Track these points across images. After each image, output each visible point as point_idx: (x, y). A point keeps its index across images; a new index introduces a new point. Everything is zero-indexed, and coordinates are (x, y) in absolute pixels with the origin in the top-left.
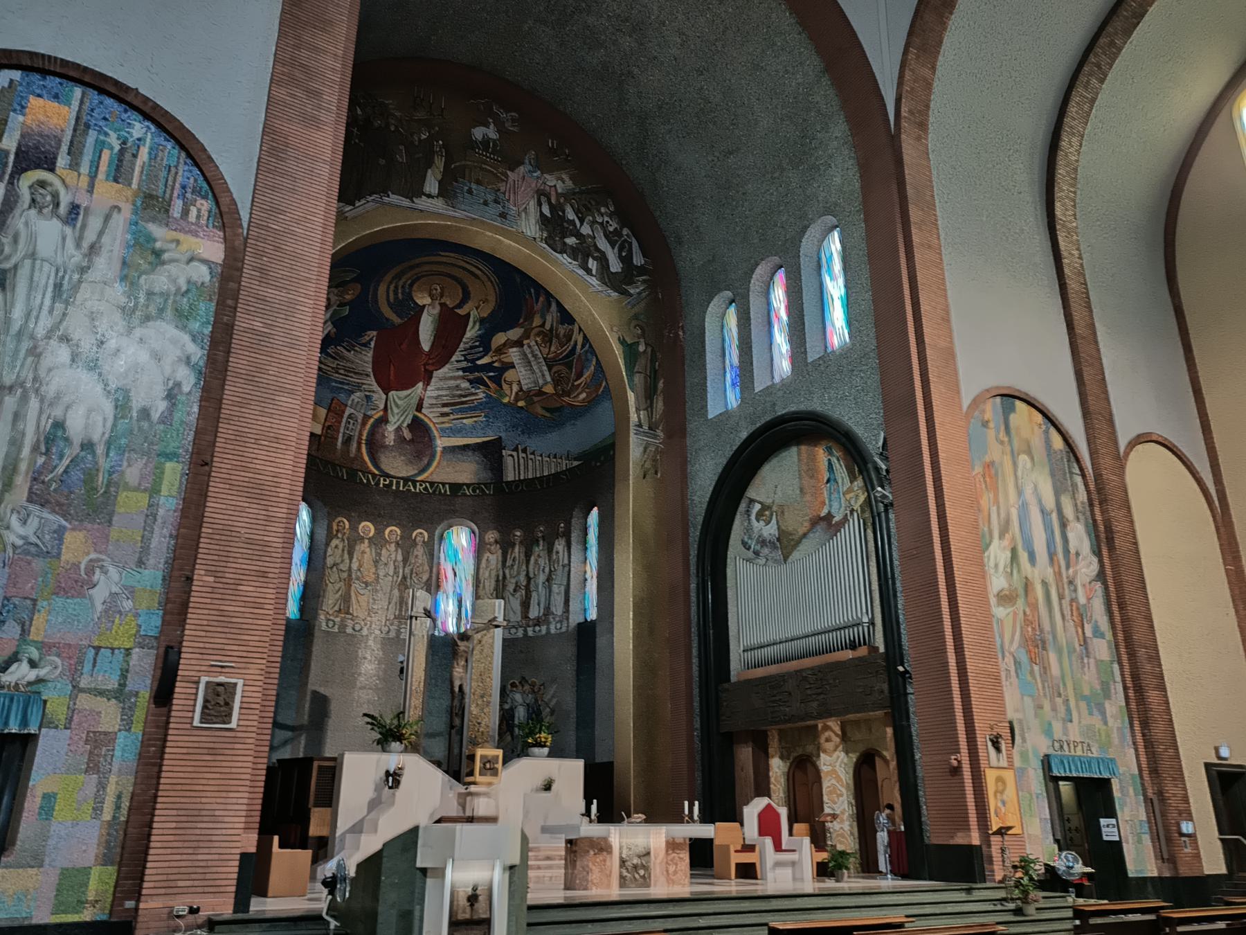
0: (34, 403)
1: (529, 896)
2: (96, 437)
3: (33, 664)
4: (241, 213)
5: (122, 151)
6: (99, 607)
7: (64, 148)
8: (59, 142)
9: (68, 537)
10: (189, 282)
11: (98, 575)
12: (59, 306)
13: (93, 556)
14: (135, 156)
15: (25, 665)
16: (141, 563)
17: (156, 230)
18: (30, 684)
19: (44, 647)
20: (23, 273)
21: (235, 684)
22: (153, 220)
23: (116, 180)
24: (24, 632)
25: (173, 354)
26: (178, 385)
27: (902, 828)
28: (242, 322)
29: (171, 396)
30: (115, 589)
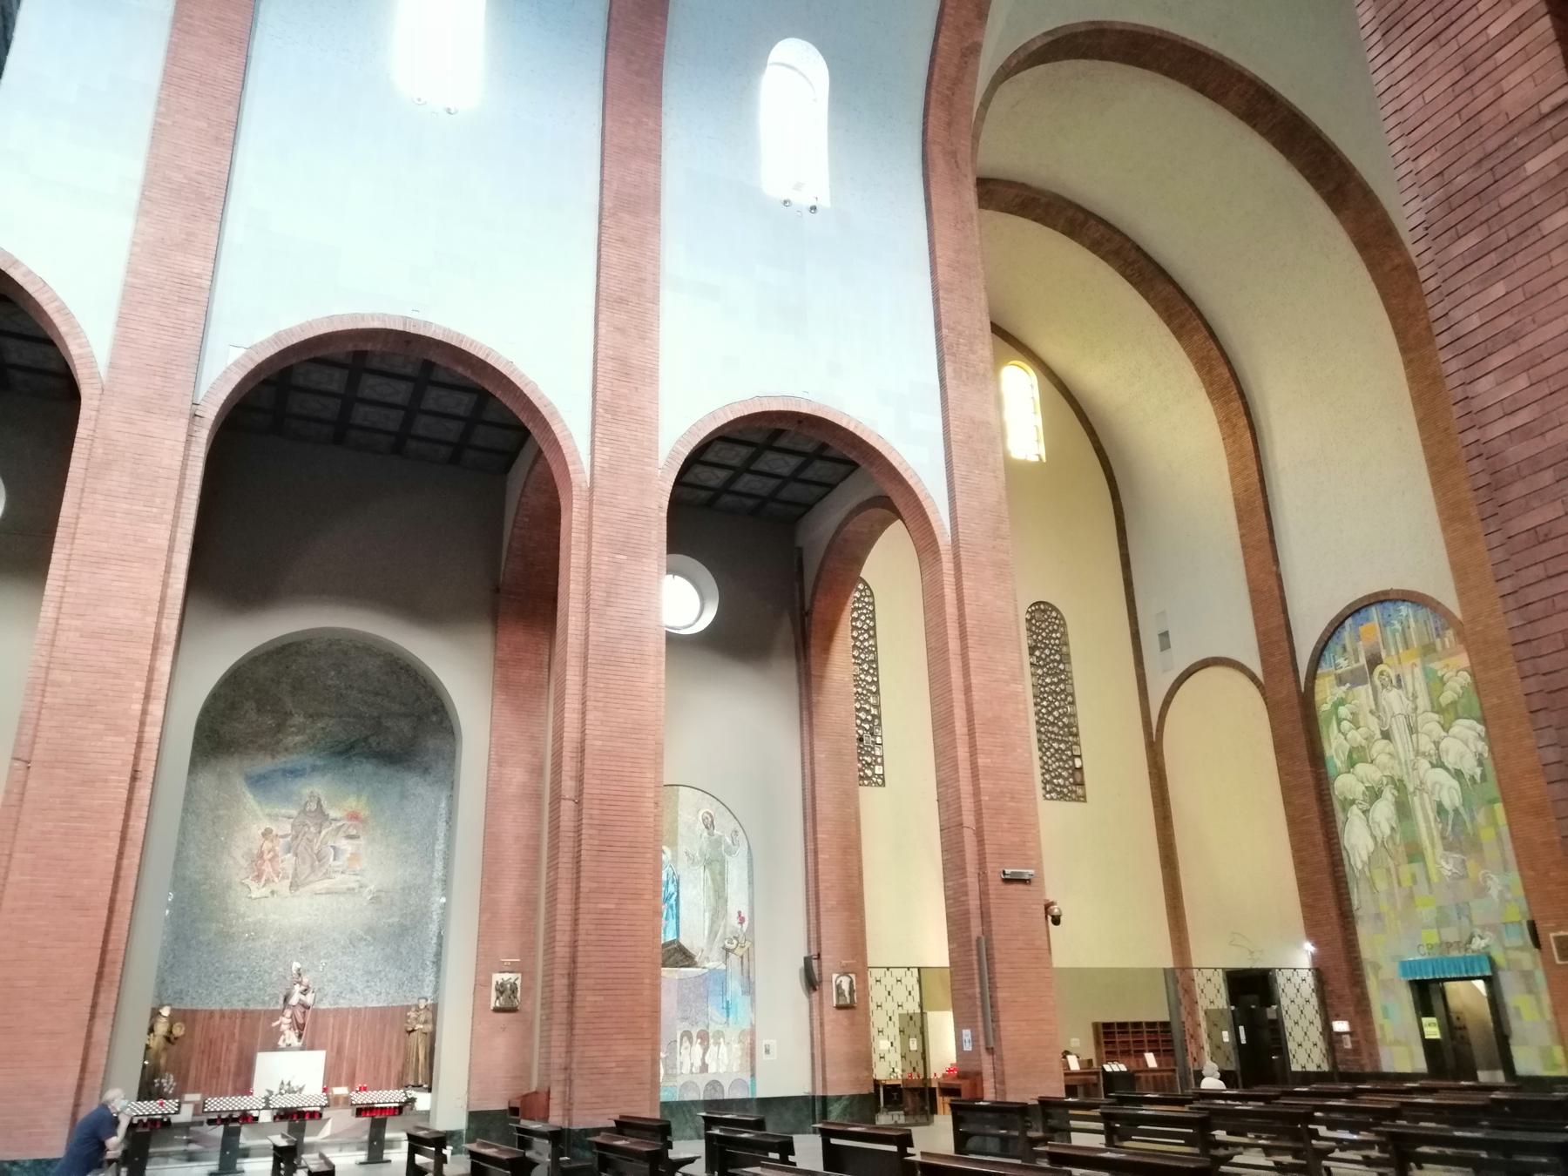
0: (1425, 795)
1: (662, 1094)
2: (1457, 805)
3: (1481, 938)
4: (581, 456)
5: (1403, 629)
6: (1497, 900)
7: (1381, 645)
8: (1378, 644)
9: (1468, 864)
10: (1461, 687)
11: (1489, 882)
12: (1414, 736)
13: (1482, 872)
14: (1409, 627)
15: (1478, 939)
16: (1506, 870)
17: (1436, 665)
18: (1484, 948)
19: (1483, 927)
20: (1394, 727)
21: (1557, 939)
22: (1432, 661)
23: (1407, 648)
24: (1471, 921)
25: (1471, 735)
26: (1481, 754)
27: (433, 1149)
28: (188, 472)
29: (1480, 763)
30: (1500, 888)
